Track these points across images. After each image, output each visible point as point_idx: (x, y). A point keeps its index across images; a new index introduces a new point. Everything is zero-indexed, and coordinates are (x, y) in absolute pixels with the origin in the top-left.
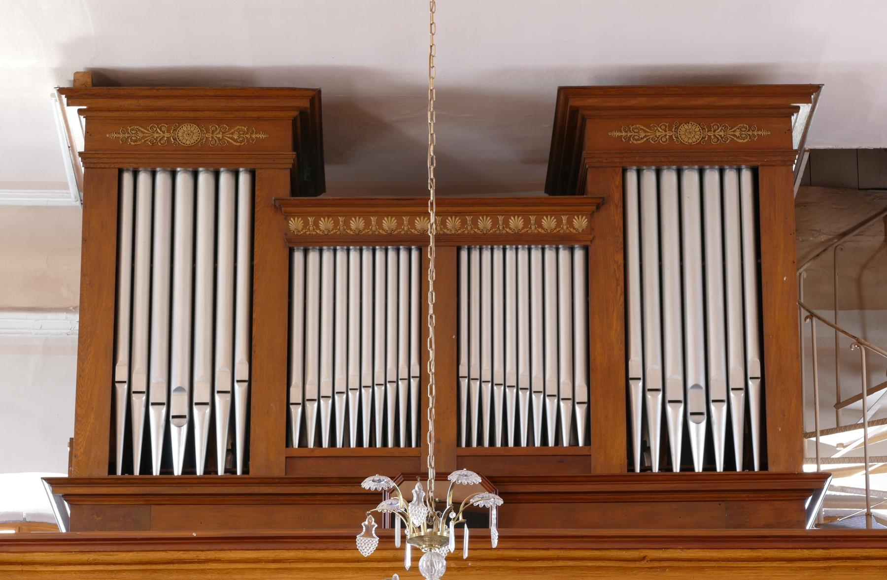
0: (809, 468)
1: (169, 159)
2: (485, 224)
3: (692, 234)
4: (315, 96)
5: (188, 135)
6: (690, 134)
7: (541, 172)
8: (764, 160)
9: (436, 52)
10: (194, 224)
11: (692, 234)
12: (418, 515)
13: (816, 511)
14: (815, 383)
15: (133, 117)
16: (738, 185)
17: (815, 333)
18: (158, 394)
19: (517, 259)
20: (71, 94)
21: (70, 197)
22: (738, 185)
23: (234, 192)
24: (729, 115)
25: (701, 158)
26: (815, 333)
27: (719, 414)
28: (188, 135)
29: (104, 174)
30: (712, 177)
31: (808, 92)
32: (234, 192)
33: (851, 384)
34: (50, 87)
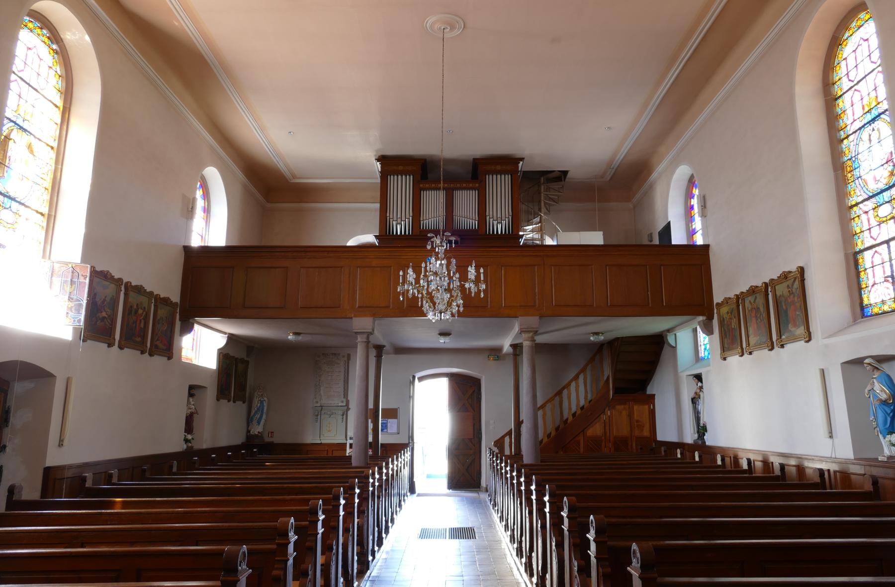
0: (521, 233)
1: (397, 173)
2: (458, 185)
3: (499, 188)
4: (425, 160)
5: (401, 168)
6: (499, 167)
7: (470, 175)
8: (513, 172)
9: (40, 211)
10: (402, 186)
11: (499, 188)
12: (438, 242)
13: (522, 242)
14: (523, 216)
15: (391, 164)
16: (508, 178)
17: (523, 207)
18: (395, 219)
19: (465, 192)
20: (378, 160)
21: (379, 180)
22: (508, 178)
23: (409, 179)
24: (505, 164)
25: (500, 172)
26: (523, 207)
27: (504, 222)
28: (401, 168)
29: (384, 175)
30: (499, 176)
31: (522, 159)
32: (409, 179)
33: (530, 217)
34: (374, 159)
